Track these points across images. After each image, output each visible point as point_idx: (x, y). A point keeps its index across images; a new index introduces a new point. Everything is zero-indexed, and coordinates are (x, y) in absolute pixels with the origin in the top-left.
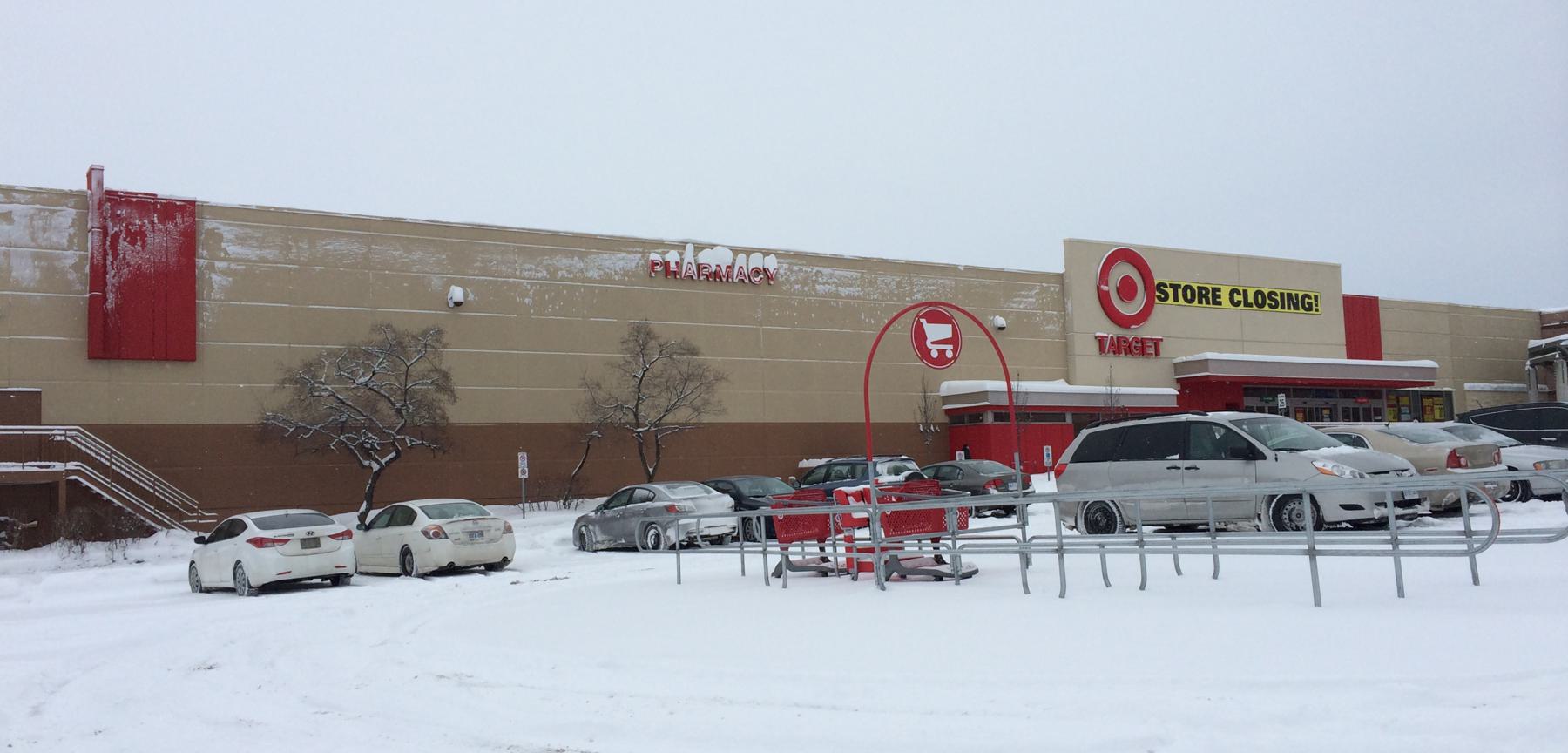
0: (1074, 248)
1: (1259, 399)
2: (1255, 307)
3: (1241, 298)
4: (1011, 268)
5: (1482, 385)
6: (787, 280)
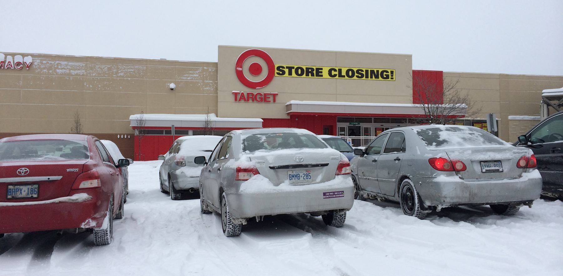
0: (222, 49)
1: (349, 123)
2: (346, 77)
3: (337, 73)
4: (553, 75)
5: (522, 117)
6: (39, 68)
